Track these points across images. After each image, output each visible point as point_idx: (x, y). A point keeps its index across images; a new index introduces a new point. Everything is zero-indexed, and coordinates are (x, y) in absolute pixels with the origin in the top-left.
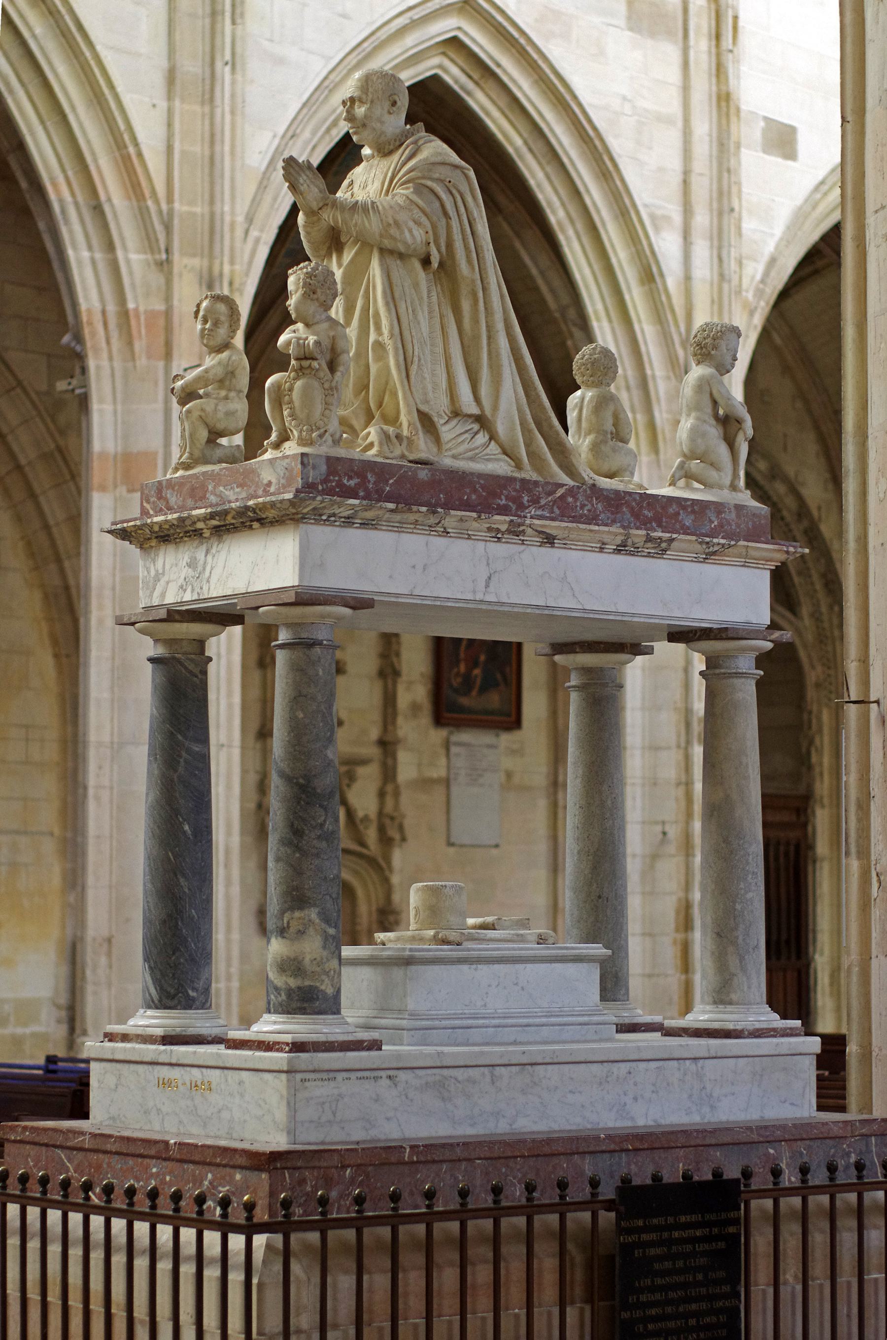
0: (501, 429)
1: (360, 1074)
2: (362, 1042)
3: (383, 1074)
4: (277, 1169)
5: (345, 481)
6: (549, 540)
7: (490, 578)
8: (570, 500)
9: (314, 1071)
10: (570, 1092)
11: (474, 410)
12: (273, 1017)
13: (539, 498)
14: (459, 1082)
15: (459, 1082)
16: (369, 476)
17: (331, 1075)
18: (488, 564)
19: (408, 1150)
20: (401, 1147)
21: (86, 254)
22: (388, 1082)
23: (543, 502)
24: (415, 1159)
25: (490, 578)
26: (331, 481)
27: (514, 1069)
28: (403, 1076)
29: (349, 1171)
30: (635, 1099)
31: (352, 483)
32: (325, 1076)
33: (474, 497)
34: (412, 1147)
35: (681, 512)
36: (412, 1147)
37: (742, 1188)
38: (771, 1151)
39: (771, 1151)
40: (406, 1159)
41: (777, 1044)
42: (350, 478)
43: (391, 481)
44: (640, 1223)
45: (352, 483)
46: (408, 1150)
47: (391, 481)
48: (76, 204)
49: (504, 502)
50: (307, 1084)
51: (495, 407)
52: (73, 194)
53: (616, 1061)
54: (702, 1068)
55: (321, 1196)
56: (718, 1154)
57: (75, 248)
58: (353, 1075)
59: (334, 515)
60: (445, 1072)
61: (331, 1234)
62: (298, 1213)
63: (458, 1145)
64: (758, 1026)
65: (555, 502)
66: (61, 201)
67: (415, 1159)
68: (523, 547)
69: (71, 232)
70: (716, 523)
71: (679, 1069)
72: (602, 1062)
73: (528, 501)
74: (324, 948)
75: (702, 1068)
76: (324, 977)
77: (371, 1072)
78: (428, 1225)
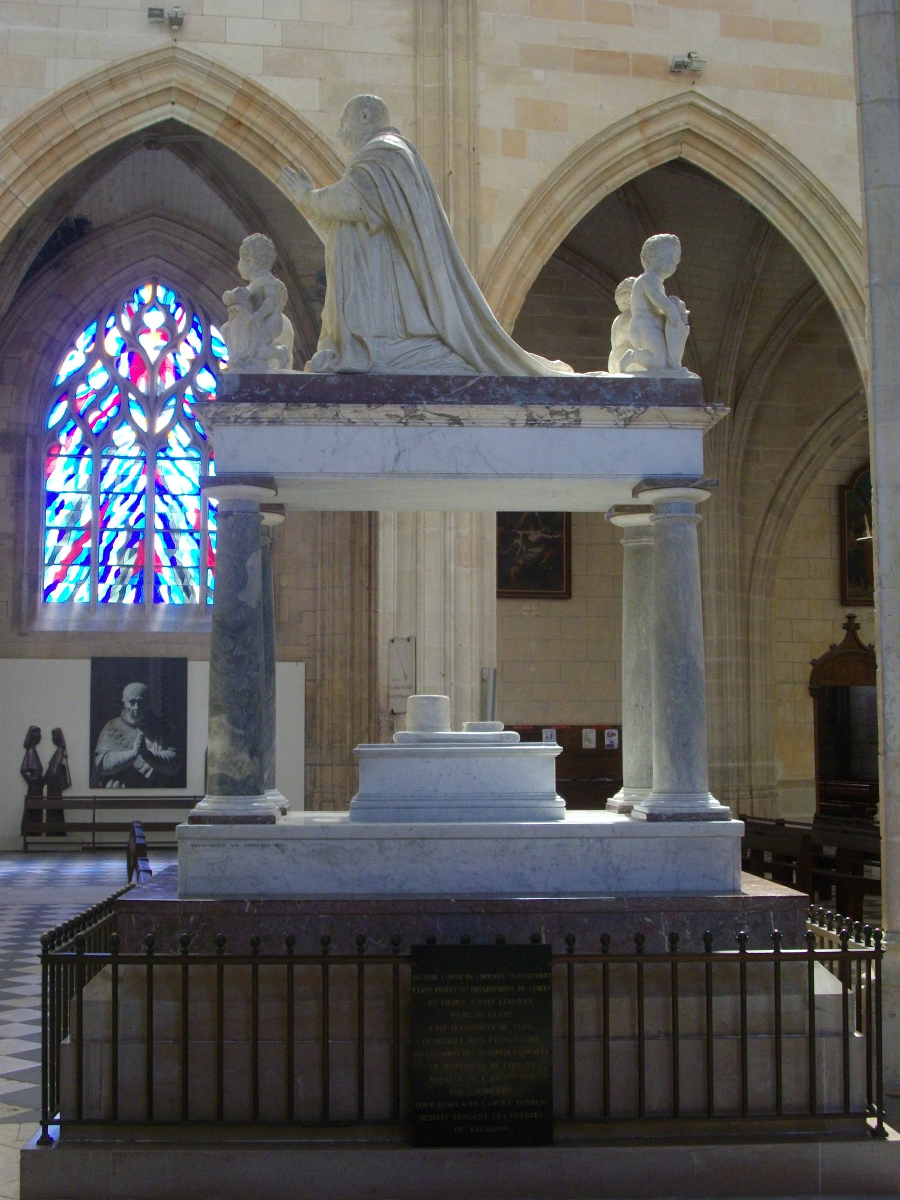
0: (451, 340)
1: (248, 842)
2: (257, 817)
3: (271, 843)
4: (122, 913)
5: (257, 392)
6: (456, 421)
7: (399, 455)
8: (481, 388)
9: (203, 839)
10: (463, 862)
11: (430, 330)
12: (215, 798)
13: (449, 388)
14: (347, 851)
15: (347, 851)
16: (280, 386)
17: (221, 842)
18: (397, 444)
19: (248, 904)
20: (243, 901)
21: (861, 338)
22: (275, 849)
23: (453, 392)
24: (255, 911)
25: (399, 455)
26: (244, 393)
27: (403, 842)
28: (290, 845)
29: (192, 918)
30: (534, 870)
31: (264, 392)
32: (214, 842)
33: (383, 393)
34: (252, 902)
35: (601, 389)
36: (252, 902)
37: (873, 949)
38: (648, 920)
39: (648, 920)
40: (247, 911)
41: (692, 828)
42: (262, 389)
43: (301, 388)
44: (435, 977)
45: (264, 392)
46: (248, 904)
47: (301, 388)
48: (852, 310)
49: (413, 395)
50: (197, 848)
51: (444, 328)
52: (849, 305)
53: (512, 838)
54: (609, 846)
55: (149, 937)
56: (586, 920)
57: (853, 336)
58: (241, 843)
59: (237, 417)
60: (331, 842)
61: (332, 967)
62: (334, 949)
63: (299, 902)
64: (678, 810)
65: (465, 391)
66: (842, 310)
67: (255, 911)
68: (431, 429)
69: (850, 327)
70: (640, 395)
71: (582, 846)
72: (497, 839)
73: (438, 392)
74: (232, 744)
75: (609, 846)
76: (231, 767)
77: (260, 843)
78: (569, 965)
